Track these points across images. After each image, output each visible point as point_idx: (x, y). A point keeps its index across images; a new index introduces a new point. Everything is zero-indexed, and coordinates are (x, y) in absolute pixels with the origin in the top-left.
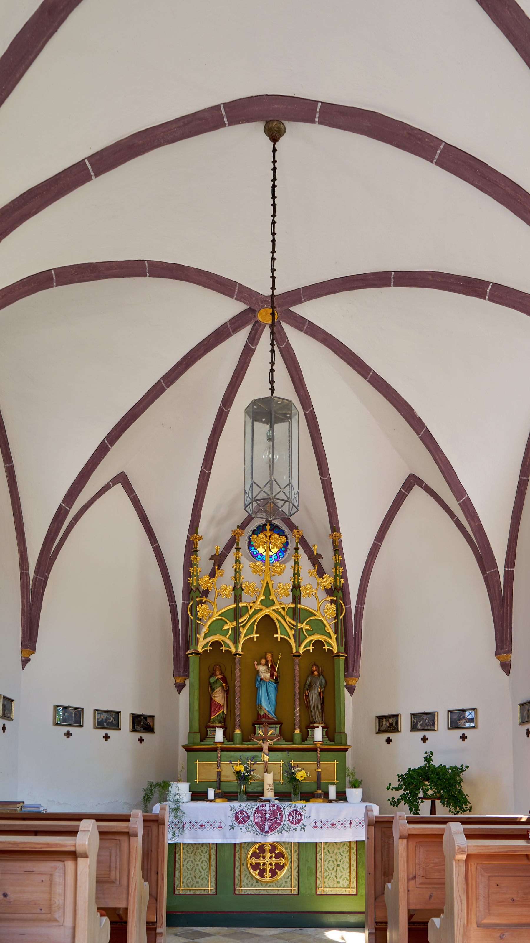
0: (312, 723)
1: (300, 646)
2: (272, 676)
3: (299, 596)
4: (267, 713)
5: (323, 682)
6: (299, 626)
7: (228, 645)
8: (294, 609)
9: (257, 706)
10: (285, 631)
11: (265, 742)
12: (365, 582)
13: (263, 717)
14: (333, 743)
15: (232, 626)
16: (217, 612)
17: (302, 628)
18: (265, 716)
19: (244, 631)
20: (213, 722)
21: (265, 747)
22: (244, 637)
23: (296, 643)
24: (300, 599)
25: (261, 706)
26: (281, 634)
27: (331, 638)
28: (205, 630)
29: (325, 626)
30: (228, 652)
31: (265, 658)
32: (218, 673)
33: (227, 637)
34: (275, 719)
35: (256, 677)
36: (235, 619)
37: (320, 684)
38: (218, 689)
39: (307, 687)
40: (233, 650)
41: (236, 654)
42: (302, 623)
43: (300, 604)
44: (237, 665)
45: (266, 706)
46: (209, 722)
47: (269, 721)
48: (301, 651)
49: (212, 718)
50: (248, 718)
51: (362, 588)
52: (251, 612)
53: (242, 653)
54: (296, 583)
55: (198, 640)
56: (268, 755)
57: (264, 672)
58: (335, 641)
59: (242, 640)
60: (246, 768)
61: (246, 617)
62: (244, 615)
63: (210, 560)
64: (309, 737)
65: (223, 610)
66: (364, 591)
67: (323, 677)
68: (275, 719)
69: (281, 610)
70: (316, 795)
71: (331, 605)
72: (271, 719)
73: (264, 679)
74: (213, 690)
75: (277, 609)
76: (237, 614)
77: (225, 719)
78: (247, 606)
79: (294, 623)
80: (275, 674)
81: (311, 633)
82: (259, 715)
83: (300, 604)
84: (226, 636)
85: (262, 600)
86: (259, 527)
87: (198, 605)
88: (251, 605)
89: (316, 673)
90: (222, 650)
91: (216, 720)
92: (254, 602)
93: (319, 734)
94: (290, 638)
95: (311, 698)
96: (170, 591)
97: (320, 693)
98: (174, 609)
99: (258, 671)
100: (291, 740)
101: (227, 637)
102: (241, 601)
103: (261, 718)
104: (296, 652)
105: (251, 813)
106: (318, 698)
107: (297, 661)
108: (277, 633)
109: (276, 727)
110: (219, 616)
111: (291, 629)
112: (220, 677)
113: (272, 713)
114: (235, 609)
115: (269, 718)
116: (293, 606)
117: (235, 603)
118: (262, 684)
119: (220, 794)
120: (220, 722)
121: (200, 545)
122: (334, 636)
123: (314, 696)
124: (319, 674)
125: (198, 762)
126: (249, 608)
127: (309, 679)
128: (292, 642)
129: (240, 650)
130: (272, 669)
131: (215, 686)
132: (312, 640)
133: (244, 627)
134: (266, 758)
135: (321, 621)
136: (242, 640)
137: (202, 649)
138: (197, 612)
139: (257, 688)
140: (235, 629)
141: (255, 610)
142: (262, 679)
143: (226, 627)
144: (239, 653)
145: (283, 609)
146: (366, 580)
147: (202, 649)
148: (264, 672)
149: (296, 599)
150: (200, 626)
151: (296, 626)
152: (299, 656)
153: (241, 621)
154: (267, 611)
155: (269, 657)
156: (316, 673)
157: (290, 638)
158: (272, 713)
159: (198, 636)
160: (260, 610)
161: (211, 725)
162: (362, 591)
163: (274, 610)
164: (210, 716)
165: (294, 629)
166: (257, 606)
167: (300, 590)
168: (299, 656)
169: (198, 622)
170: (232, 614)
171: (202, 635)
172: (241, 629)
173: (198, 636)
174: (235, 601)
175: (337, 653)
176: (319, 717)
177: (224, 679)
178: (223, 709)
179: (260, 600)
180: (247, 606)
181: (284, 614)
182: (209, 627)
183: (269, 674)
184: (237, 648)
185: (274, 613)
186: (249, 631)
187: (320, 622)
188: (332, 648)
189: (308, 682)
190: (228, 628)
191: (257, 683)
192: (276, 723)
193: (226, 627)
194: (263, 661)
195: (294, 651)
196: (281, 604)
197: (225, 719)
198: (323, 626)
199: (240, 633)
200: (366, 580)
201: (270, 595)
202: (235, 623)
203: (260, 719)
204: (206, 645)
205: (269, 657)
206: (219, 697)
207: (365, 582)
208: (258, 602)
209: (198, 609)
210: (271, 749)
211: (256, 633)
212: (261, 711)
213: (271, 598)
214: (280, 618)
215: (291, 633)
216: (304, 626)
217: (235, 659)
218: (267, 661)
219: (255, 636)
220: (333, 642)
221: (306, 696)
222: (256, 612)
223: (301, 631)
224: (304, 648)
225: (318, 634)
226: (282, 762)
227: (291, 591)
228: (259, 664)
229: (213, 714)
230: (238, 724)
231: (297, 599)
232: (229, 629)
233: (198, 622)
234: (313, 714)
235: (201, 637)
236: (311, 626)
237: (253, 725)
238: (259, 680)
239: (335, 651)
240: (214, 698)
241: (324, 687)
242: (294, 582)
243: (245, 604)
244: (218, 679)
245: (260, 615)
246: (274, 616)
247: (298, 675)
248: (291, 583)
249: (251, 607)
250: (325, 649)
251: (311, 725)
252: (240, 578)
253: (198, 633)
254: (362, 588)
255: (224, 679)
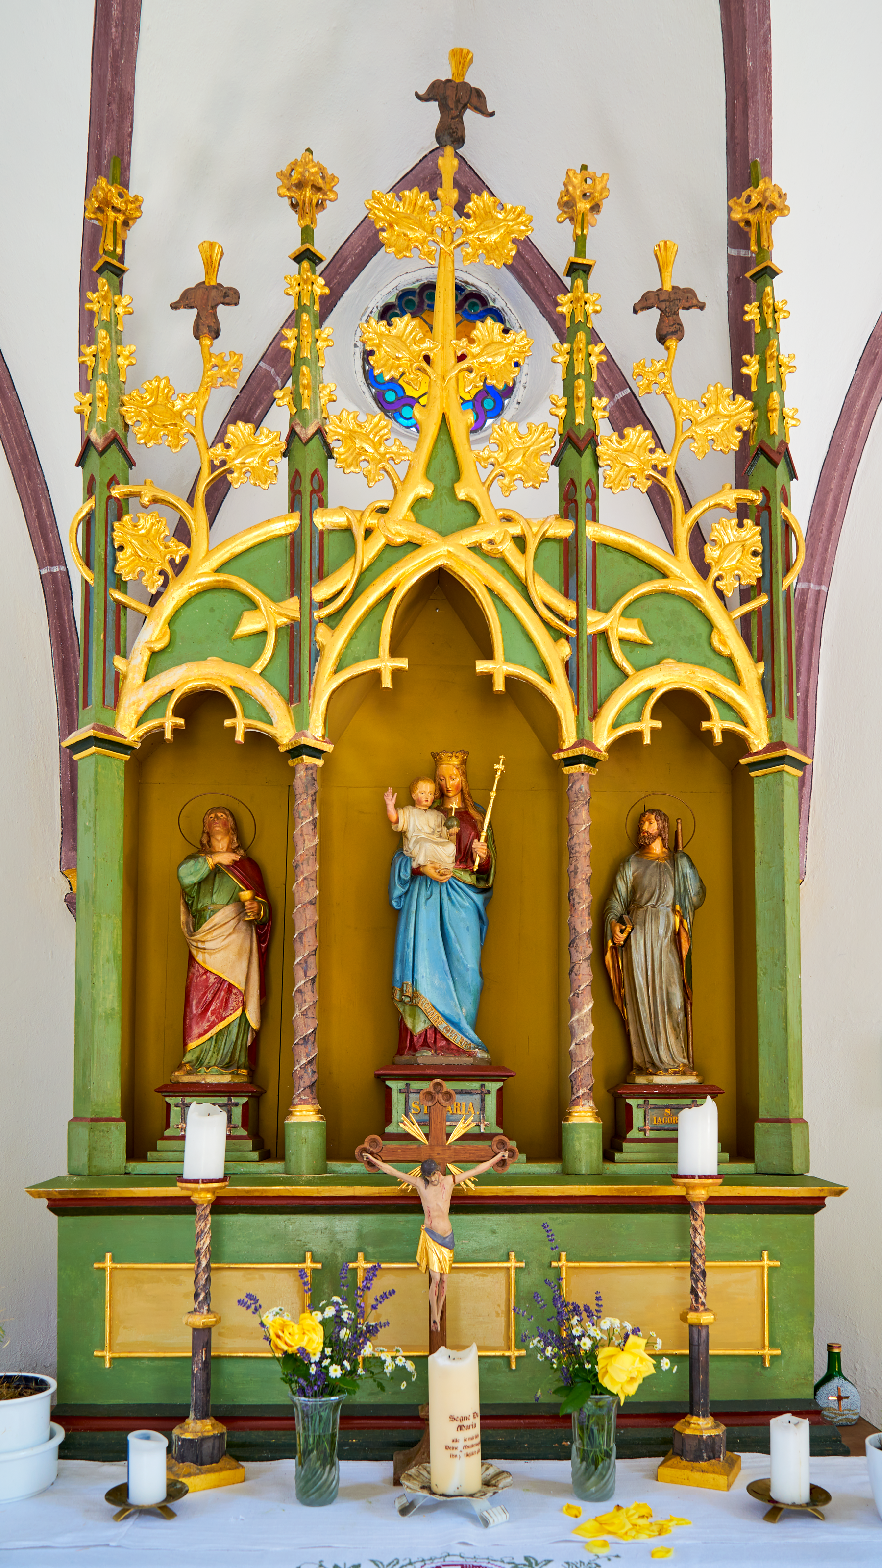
0: (642, 1071)
1: (594, 716)
2: (464, 856)
3: (593, 485)
4: (442, 1026)
5: (693, 887)
6: (594, 622)
7: (262, 708)
8: (569, 548)
9: (391, 995)
10: (525, 648)
11: (436, 1177)
12: (840, 487)
13: (425, 1044)
14: (748, 1167)
15: (282, 621)
16: (209, 552)
17: (604, 634)
18: (433, 1038)
19: (333, 642)
20: (200, 1061)
21: (437, 1198)
22: (339, 668)
23: (577, 702)
24: (593, 498)
25: (415, 994)
26: (507, 660)
27: (737, 679)
28: (152, 634)
29: (711, 626)
30: (260, 741)
31: (435, 777)
32: (221, 842)
33: (258, 668)
34: (481, 1054)
35: (392, 863)
36: (295, 588)
37: (680, 896)
38: (218, 918)
39: (617, 907)
40: (284, 733)
41: (299, 751)
42: (607, 611)
43: (595, 519)
44: (303, 802)
45: (440, 994)
46: (180, 1066)
47: (452, 1060)
48: (603, 737)
49: (192, 1045)
50: (355, 1047)
51: (828, 509)
52: (368, 552)
53: (328, 748)
54: (579, 420)
55: (115, 684)
56: (447, 1243)
57: (430, 843)
58: (757, 692)
59: (326, 683)
60: (332, 1325)
61: (344, 578)
62: (339, 565)
63: (175, 306)
64: (633, 1134)
65: (237, 547)
66: (832, 522)
67: (692, 866)
68: (481, 1054)
69: (508, 549)
70: (690, 1446)
71: (741, 525)
72: (459, 1051)
73: (430, 871)
74: (198, 918)
75: (491, 542)
76: (301, 560)
77: (253, 1052)
78: (348, 530)
79: (568, 609)
80: (480, 848)
81: (645, 654)
82: (403, 1031)
83: (595, 519)
84: (250, 664)
85: (420, 501)
86: (405, 295)
87: (119, 518)
88: (371, 521)
89: (657, 847)
90: (233, 729)
91: (211, 1058)
92: (383, 510)
93: (699, 1134)
94: (550, 680)
95: (638, 957)
96: (39, 515)
97: (677, 936)
98: (56, 593)
99: (401, 836)
100: (551, 1146)
101: (258, 668)
102: (322, 504)
103: (414, 1049)
104: (580, 743)
105: (473, 456)
106: (669, 960)
107: (582, 785)
108: (489, 654)
109: (483, 1093)
110: (217, 571)
111: (557, 635)
112: (226, 858)
113: (465, 1025)
114: (294, 540)
115: (451, 1048)
116: (565, 529)
117: (292, 508)
118: (420, 892)
119: (207, 1447)
120: (228, 1065)
121: (140, 247)
122: (752, 671)
123: (650, 945)
124: (674, 851)
125: (108, 1264)
126: (359, 533)
127: (630, 872)
128: (559, 694)
129: (315, 733)
130: (465, 824)
131: (205, 902)
132: (651, 691)
133: (334, 620)
134: (438, 1258)
135: (692, 601)
136: (326, 683)
137: (139, 723)
138: (113, 551)
139: (397, 914)
140: (292, 635)
141: (388, 546)
142: (417, 873)
143: (249, 625)
144: (311, 743)
145: (520, 541)
146: (842, 477)
147: (139, 723)
148: (430, 843)
149: (575, 500)
150: (128, 621)
151: (577, 623)
152: (591, 761)
153: (321, 593)
154: (437, 553)
155: (451, 771)
156: (657, 847)
157: (550, 680)
158: (465, 1025)
159: (119, 662)
160: (412, 546)
161: (186, 1079)
162: (825, 522)
163: (476, 549)
164: (186, 1035)
165: (568, 638)
166: (399, 527)
167: (596, 458)
168: (591, 761)
169: (118, 595)
170: (282, 563)
171: (139, 658)
172: (322, 633)
173: (119, 662)
174: (294, 504)
175: (769, 748)
176: (672, 1040)
177: (250, 871)
178: (244, 1003)
179: (410, 499)
180: (348, 530)
181: (521, 564)
182: (171, 622)
183: (452, 849)
184: (301, 723)
185: (475, 561)
186: (363, 642)
187: (686, 608)
188: (746, 725)
189: (622, 886)
190: (258, 627)
191: (399, 891)
192: (480, 1073)
193: (249, 625)
194: (425, 790)
195: (569, 736)
196: (508, 519)
197: (253, 1052)
198: (703, 629)
199: (316, 654)
200: (842, 477)
201: (457, 476)
202: (292, 607)
203: (404, 1049)
204: (155, 707)
205: (451, 771)
206: (224, 950)
207: (840, 487)
208: (403, 509)
209: (118, 537)
210: (461, 1204)
211: (394, 652)
212: (413, 1016)
213: (461, 495)
214: (503, 586)
215: (557, 654)
216: (620, 626)
217: (293, 771)
218: (442, 794)
219: (387, 664)
220: (751, 702)
221: (615, 947)
222: (395, 551)
223: (600, 646)
224: (615, 726)
225: (680, 661)
226: (513, 1264)
227: (556, 462)
228: (408, 800)
229: (196, 1031)
230: (308, 1078)
231: (582, 496)
232: (264, 632)
233: (118, 595)
234: (647, 1028)
235: (132, 666)
236: (645, 626)
237: (381, 1079)
238: (406, 875)
239: (759, 739)
240: (200, 957)
241: (696, 908)
242: (568, 420)
243: (340, 520)
244: (217, 870)
245: (408, 573)
246: (475, 575)
247: (587, 848)
248: (555, 424)
249: (368, 532)
250: (710, 733)
251: (640, 1080)
252: (316, 394)
253: (121, 650)
254: (828, 509)
255: (250, 871)
